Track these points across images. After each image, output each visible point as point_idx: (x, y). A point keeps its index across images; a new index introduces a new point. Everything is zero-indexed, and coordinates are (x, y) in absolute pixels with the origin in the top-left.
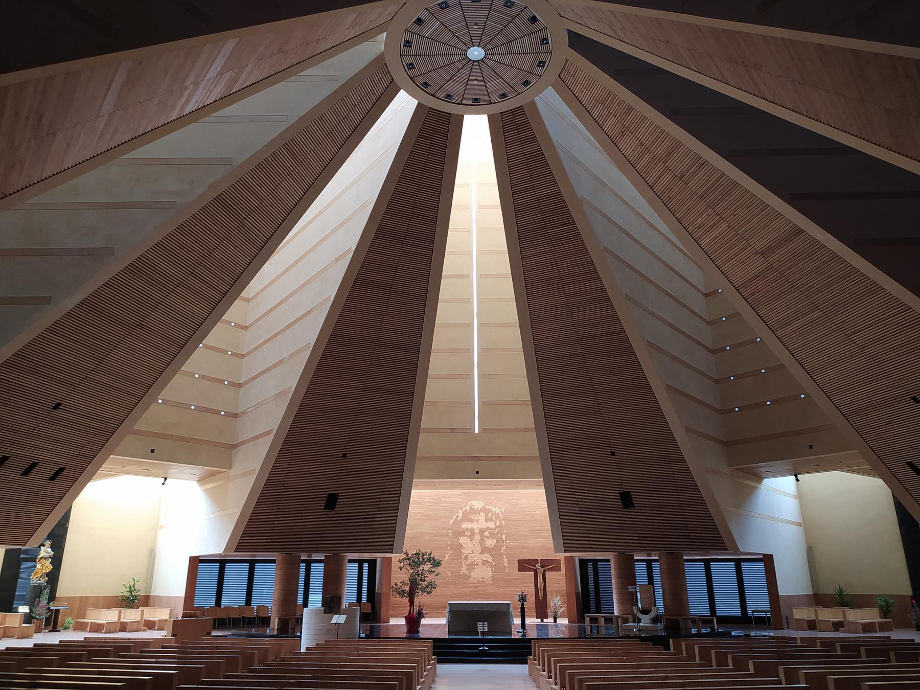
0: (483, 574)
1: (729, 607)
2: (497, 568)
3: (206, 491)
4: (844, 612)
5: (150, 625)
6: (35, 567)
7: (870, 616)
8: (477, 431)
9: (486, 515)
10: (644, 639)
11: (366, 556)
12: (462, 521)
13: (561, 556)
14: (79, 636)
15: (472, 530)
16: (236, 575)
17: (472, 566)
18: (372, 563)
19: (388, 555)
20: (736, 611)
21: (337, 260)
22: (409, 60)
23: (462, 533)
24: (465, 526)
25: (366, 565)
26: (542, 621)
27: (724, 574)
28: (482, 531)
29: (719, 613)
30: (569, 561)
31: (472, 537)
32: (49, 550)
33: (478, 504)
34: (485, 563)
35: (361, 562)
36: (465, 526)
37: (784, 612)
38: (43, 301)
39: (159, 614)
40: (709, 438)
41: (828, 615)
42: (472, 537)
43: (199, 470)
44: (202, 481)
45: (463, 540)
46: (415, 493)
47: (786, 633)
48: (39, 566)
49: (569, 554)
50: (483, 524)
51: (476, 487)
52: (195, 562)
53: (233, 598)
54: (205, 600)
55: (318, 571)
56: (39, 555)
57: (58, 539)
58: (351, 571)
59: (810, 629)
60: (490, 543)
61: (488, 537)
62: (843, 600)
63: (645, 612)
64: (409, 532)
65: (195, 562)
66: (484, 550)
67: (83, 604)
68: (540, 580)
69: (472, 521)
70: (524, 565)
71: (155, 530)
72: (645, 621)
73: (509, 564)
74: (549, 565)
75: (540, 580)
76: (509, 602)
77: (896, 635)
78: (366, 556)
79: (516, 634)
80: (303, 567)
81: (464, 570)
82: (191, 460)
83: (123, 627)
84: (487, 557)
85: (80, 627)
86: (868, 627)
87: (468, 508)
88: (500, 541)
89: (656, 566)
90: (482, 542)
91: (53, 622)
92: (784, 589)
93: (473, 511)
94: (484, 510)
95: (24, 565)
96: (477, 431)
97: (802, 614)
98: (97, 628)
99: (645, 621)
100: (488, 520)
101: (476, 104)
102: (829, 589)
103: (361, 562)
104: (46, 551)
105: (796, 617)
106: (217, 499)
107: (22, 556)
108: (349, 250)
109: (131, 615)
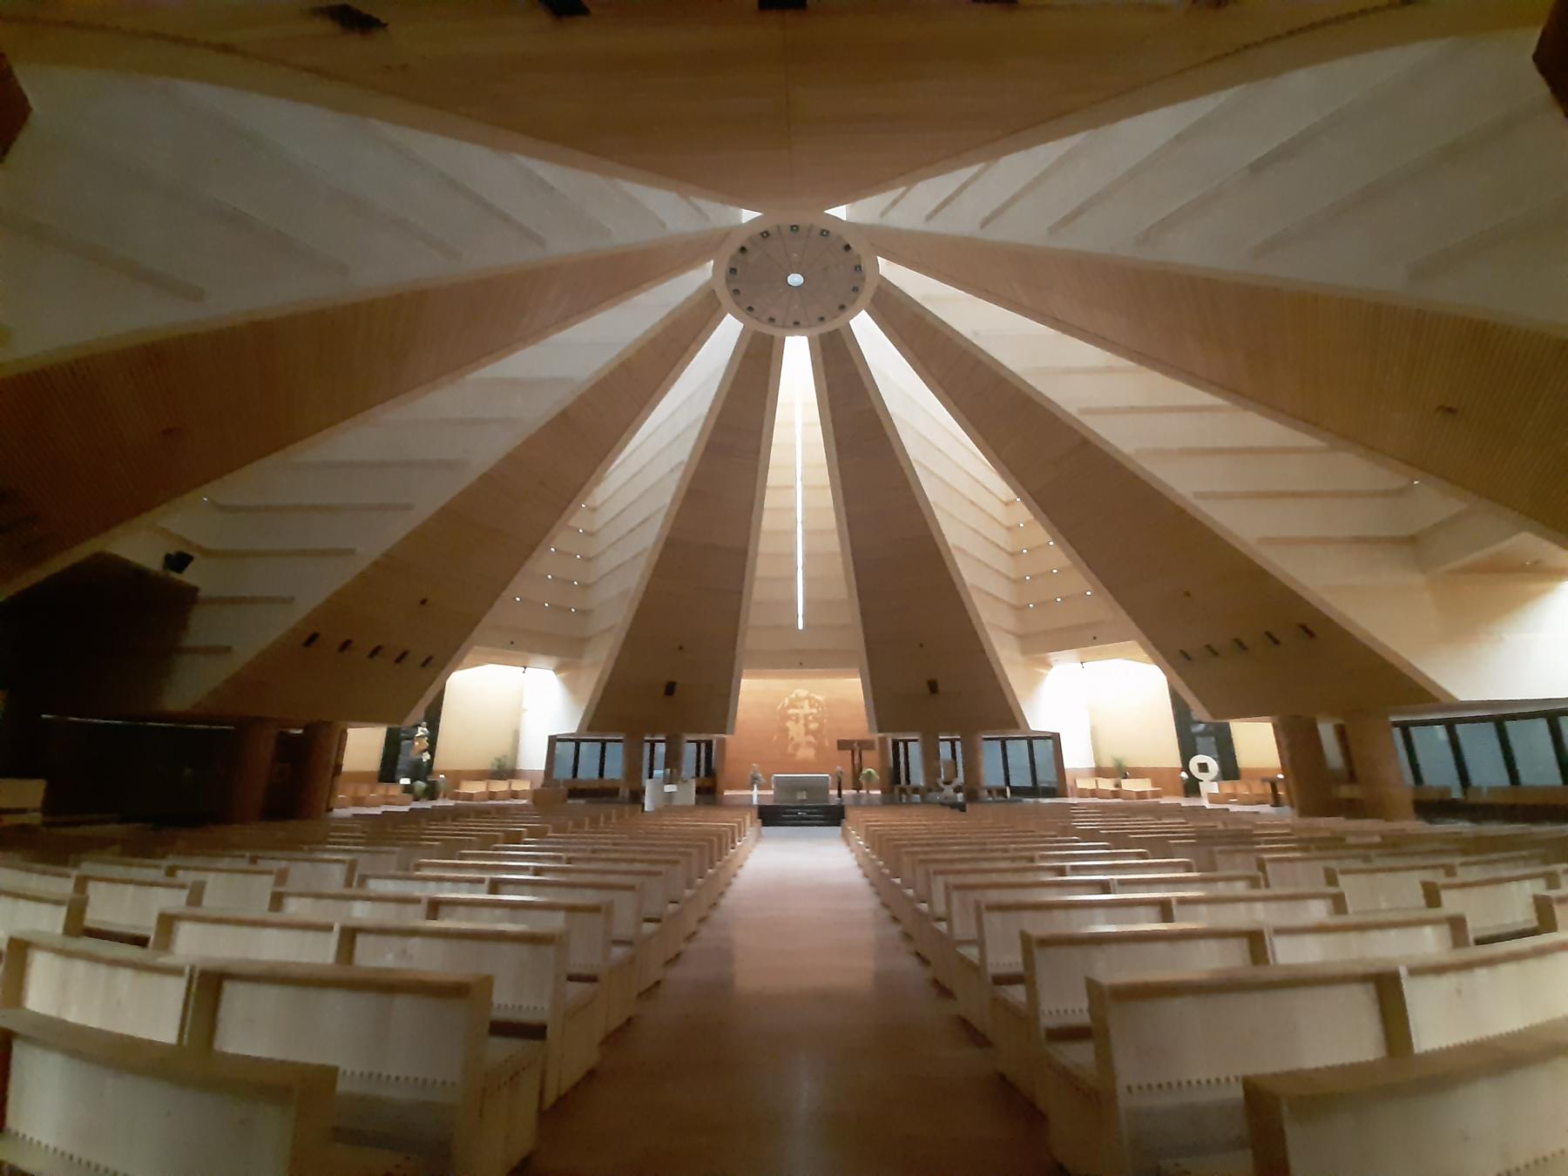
0: (807, 753)
1: (1021, 779)
2: (819, 748)
3: (559, 678)
4: (1097, 782)
5: (515, 795)
6: (413, 744)
7: (1143, 785)
8: (801, 626)
9: (810, 702)
10: (943, 804)
11: (703, 737)
12: (789, 707)
13: (877, 736)
14: (451, 803)
15: (797, 716)
16: (589, 752)
17: (797, 747)
18: (709, 744)
19: (724, 736)
20: (1029, 784)
21: (672, 471)
22: (734, 286)
23: (788, 717)
24: (791, 711)
25: (703, 746)
26: (1118, 785)
27: (1018, 751)
28: (806, 717)
29: (1012, 784)
30: (883, 741)
31: (797, 721)
32: (425, 729)
33: (803, 693)
34: (809, 744)
35: (698, 743)
36: (791, 711)
37: (1069, 782)
38: (407, 507)
39: (520, 785)
40: (1008, 632)
41: (1107, 785)
42: (797, 721)
43: (554, 661)
44: (557, 670)
45: (789, 724)
46: (744, 682)
47: (1070, 800)
48: (417, 743)
49: (881, 735)
50: (807, 709)
51: (799, 676)
52: (553, 740)
53: (588, 772)
54: (588, 772)
55: (661, 749)
56: (416, 733)
57: (433, 719)
58: (689, 751)
59: (1092, 797)
60: (813, 726)
61: (811, 721)
62: (1121, 772)
63: (947, 783)
64: (740, 707)
65: (553, 740)
66: (808, 732)
67: (458, 777)
68: (857, 757)
69: (796, 707)
70: (843, 745)
71: (519, 712)
72: (949, 790)
73: (829, 744)
74: (865, 745)
75: (857, 757)
76: (827, 775)
77: (1164, 801)
78: (703, 737)
79: (834, 801)
80: (647, 747)
81: (790, 749)
82: (546, 652)
83: (492, 796)
84: (811, 738)
85: (456, 796)
86: (1141, 795)
87: (794, 695)
88: (821, 724)
89: (958, 744)
90: (806, 726)
91: (432, 793)
92: (1069, 763)
93: (799, 699)
94: (808, 698)
95: (405, 743)
96: (801, 626)
97: (1086, 784)
98: (470, 797)
99: (949, 790)
100: (811, 706)
101: (796, 326)
102: (1108, 763)
103: (698, 743)
104: (422, 731)
105: (1079, 786)
106: (571, 686)
107: (402, 735)
108: (681, 463)
109: (500, 786)
